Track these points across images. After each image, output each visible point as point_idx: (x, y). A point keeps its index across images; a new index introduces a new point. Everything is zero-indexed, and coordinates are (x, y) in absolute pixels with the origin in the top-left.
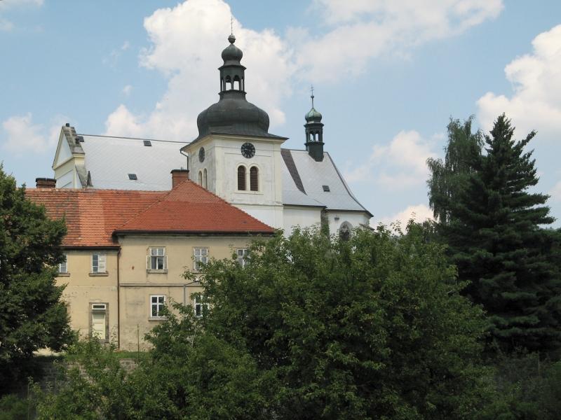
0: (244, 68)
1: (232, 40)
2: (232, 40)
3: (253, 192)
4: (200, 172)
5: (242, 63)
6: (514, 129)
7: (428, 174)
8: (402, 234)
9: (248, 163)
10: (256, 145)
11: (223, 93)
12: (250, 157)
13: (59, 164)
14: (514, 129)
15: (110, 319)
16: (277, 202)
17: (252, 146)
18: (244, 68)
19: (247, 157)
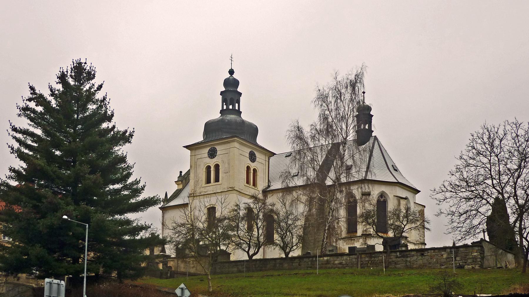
0: (240, 94)
1: (231, 72)
2: (231, 72)
3: (217, 183)
4: (209, 168)
5: (239, 89)
6: (32, 88)
7: (152, 196)
8: (178, 261)
9: (212, 163)
10: (218, 148)
11: (222, 112)
12: (214, 158)
13: (376, 142)
14: (32, 88)
15: (397, 166)
16: (230, 188)
17: (216, 148)
18: (240, 94)
19: (211, 158)
